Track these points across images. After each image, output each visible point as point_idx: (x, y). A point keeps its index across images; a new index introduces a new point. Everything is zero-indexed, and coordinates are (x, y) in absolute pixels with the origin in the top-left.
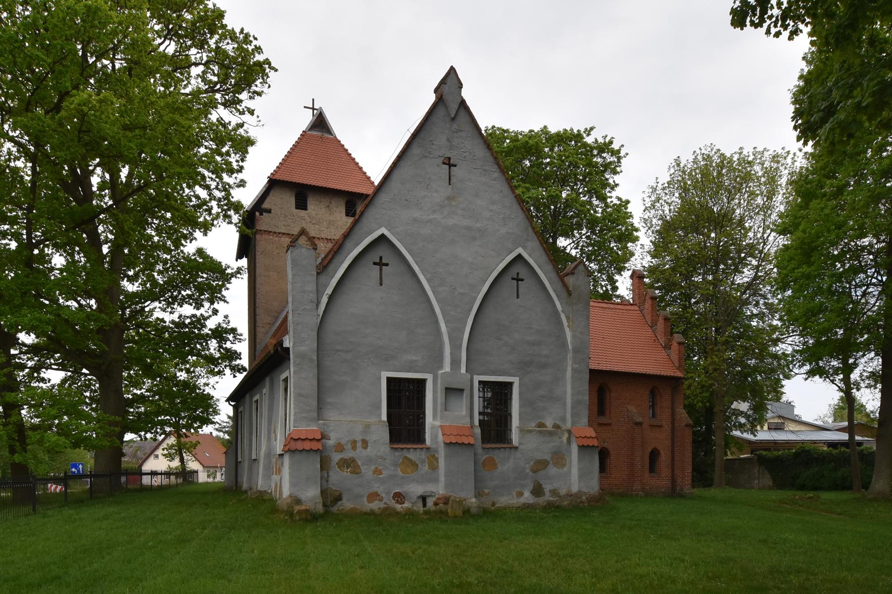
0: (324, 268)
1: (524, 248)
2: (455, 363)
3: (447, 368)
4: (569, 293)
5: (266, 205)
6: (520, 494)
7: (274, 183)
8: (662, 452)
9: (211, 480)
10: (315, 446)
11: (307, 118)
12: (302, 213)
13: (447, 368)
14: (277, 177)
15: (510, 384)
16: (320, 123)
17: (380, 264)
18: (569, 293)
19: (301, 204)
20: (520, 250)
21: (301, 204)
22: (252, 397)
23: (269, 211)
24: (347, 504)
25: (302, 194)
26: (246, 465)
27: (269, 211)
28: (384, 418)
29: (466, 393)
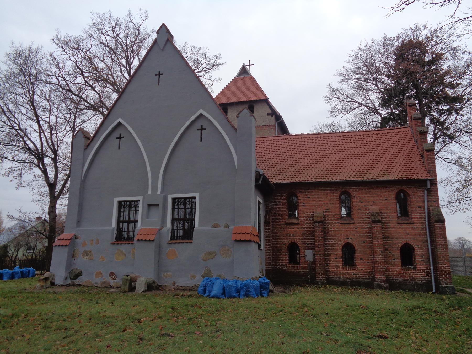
1: (204, 109)
2: (155, 188)
6: (194, 277)
8: (416, 247)
13: (150, 192)
24: (82, 280)
28: (114, 224)
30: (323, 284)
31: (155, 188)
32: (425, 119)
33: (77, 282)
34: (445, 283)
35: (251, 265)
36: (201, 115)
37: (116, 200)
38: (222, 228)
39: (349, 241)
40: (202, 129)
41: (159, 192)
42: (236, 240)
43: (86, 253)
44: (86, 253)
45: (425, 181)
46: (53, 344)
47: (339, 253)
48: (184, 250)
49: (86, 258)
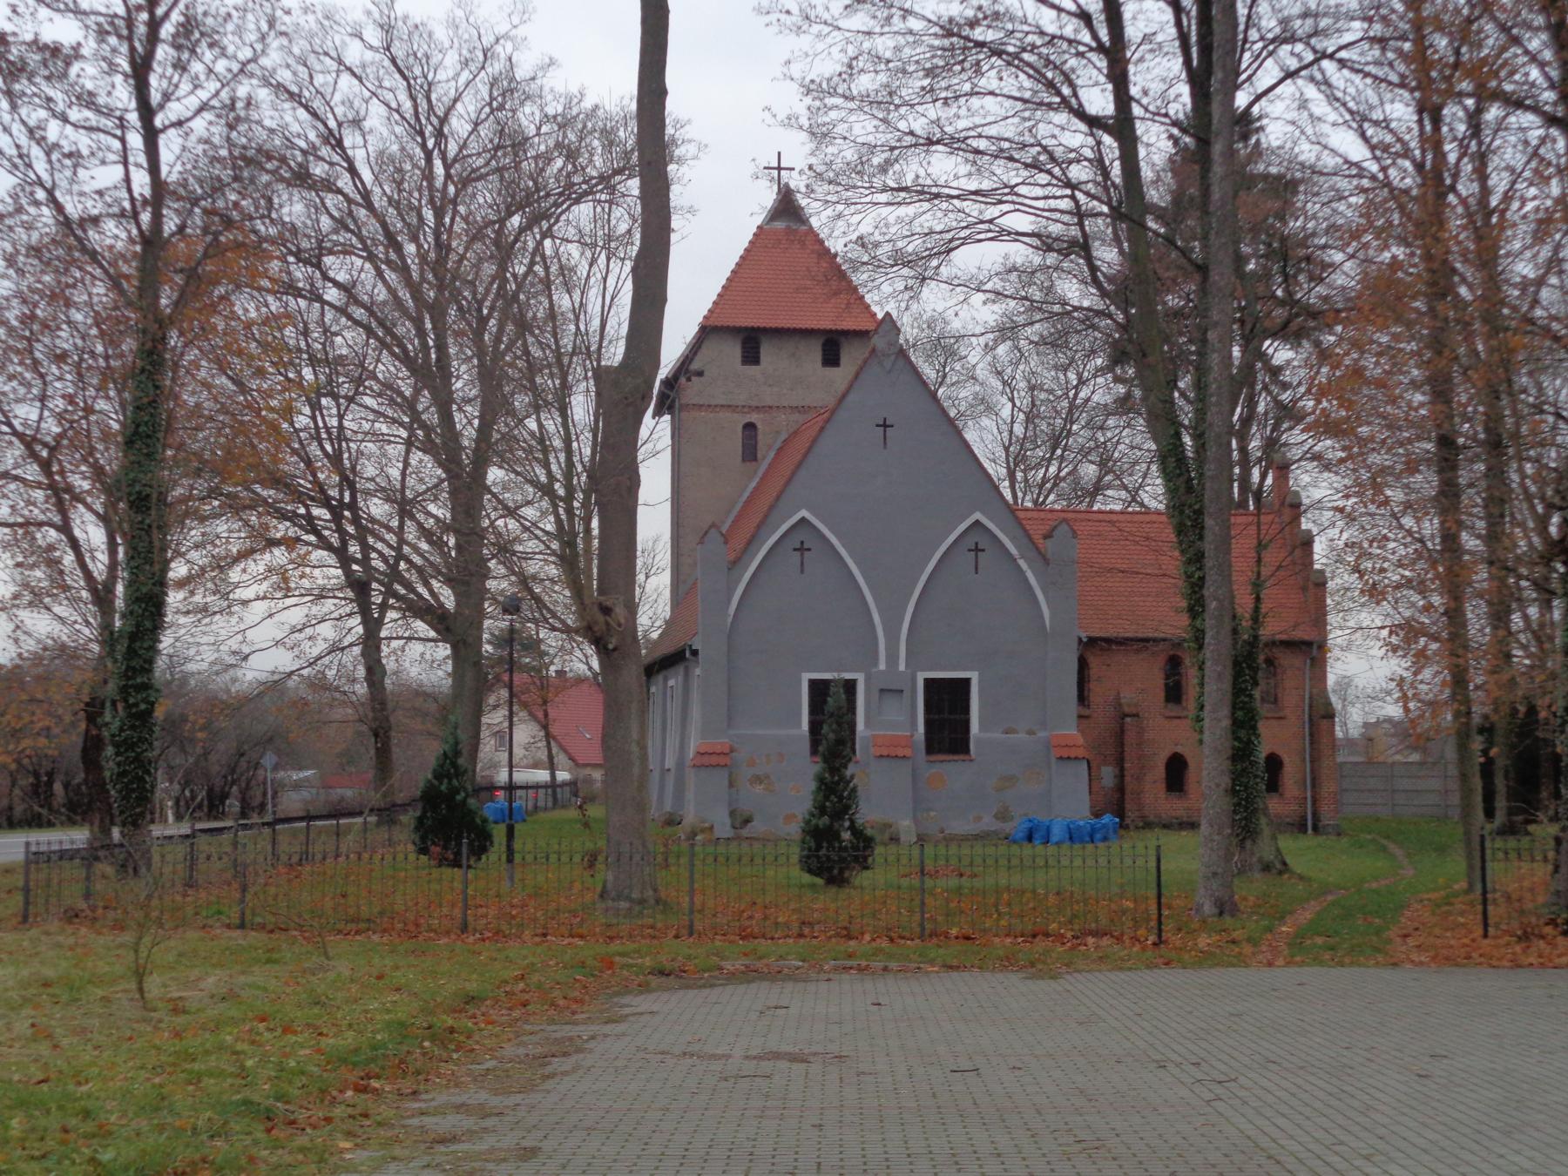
0: (736, 563)
1: (983, 513)
2: (892, 658)
3: (882, 666)
4: (1046, 561)
5: (695, 366)
6: (979, 819)
7: (708, 331)
8: (1286, 759)
9: (486, 636)
10: (722, 760)
11: (767, 197)
12: (752, 370)
13: (882, 666)
14: (710, 323)
15: (967, 681)
16: (786, 207)
17: (802, 549)
18: (1046, 561)
19: (751, 356)
20: (977, 516)
21: (751, 356)
22: (666, 680)
23: (700, 374)
24: (758, 827)
25: (751, 342)
26: (656, 776)
27: (700, 374)
28: (805, 726)
29: (907, 694)
30: (1137, 828)
31: (892, 658)
32: (1171, 492)
33: (745, 832)
34: (1327, 819)
35: (1071, 799)
36: (977, 522)
37: (806, 677)
38: (1022, 736)
39: (1179, 749)
40: (977, 550)
41: (902, 667)
42: (1061, 758)
43: (758, 779)
44: (758, 779)
45: (1309, 644)
46: (1517, 905)
47: (1160, 772)
48: (952, 771)
49: (759, 789)
